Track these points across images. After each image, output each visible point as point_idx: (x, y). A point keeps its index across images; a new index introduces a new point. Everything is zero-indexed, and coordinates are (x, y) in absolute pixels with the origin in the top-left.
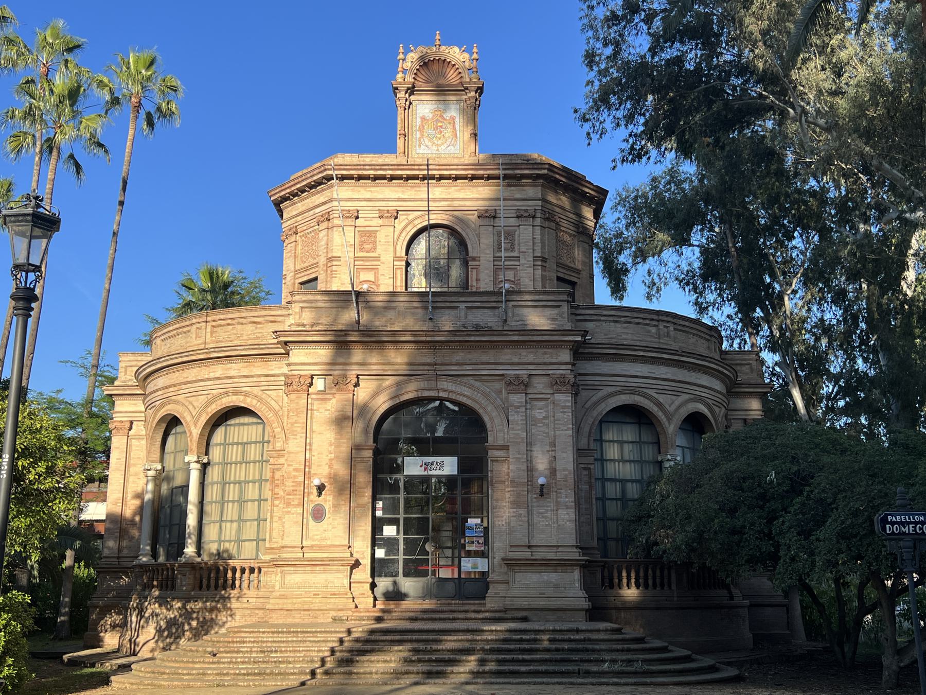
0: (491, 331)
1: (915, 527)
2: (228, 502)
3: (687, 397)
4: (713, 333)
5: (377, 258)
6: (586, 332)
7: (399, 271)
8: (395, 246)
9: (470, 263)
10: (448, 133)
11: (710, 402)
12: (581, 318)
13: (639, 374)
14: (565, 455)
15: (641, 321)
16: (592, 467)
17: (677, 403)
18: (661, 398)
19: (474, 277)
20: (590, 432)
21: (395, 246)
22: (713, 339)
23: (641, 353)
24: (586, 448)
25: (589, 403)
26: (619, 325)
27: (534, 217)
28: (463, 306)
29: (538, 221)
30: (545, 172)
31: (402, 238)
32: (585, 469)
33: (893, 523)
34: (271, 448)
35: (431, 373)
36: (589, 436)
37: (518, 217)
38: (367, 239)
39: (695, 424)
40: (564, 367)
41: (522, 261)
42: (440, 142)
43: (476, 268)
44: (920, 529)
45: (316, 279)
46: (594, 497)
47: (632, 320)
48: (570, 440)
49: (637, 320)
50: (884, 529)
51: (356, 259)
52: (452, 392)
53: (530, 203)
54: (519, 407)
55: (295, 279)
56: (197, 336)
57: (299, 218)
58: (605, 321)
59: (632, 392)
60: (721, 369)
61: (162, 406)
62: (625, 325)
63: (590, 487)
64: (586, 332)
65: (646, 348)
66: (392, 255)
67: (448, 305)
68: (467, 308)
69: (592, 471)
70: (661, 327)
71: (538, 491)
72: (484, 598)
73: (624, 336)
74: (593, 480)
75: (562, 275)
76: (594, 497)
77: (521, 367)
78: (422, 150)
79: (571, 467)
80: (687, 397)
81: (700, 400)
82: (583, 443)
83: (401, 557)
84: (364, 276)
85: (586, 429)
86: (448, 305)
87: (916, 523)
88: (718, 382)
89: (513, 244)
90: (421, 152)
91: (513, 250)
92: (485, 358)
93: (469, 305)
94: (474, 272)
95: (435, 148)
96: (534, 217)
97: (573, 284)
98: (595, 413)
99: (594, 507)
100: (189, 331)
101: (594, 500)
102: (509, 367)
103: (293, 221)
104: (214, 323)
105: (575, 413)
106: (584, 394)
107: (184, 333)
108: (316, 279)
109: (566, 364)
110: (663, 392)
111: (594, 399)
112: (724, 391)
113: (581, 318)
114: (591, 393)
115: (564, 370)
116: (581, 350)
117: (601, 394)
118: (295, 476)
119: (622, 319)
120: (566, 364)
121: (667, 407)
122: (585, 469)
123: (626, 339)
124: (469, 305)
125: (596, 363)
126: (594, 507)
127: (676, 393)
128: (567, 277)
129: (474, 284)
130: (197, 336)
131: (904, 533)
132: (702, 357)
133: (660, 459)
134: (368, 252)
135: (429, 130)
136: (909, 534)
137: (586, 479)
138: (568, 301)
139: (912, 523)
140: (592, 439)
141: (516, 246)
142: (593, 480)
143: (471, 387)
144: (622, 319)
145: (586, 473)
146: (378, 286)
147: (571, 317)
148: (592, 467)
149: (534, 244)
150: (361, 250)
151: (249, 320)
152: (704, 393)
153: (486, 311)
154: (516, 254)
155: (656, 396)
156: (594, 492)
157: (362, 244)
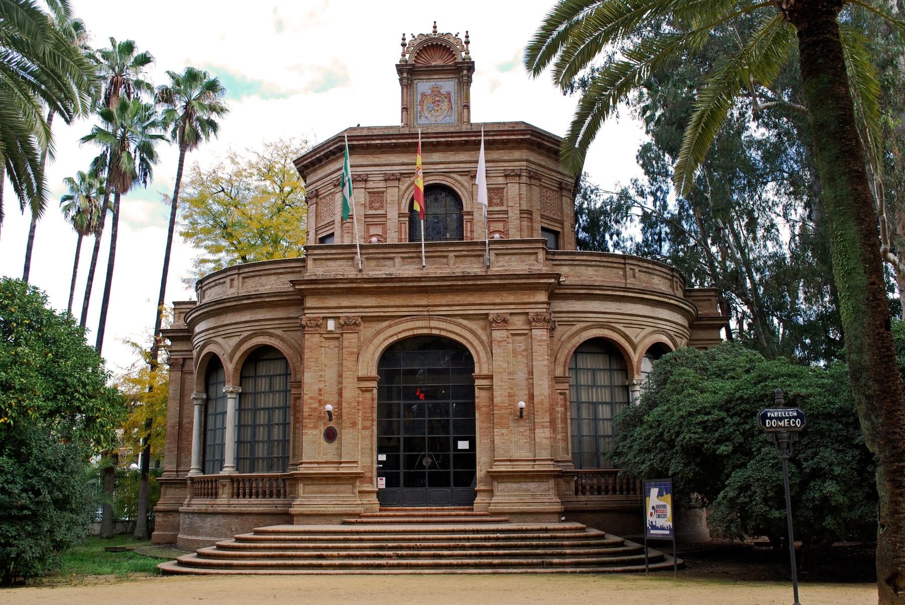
0: (476, 277)
1: (789, 421)
2: (258, 459)
3: (652, 329)
4: (675, 274)
5: (385, 216)
6: (559, 275)
7: (403, 226)
8: (399, 204)
9: (465, 217)
10: (445, 105)
11: (672, 333)
12: (558, 263)
13: (608, 311)
14: (541, 382)
15: (609, 264)
16: (567, 392)
17: (642, 335)
18: (628, 331)
19: (469, 228)
20: (565, 362)
21: (399, 204)
22: (675, 279)
23: (610, 293)
24: (562, 375)
25: (565, 337)
26: (590, 269)
27: (519, 176)
28: (452, 254)
29: (524, 179)
30: (529, 137)
31: (406, 195)
32: (561, 394)
33: (771, 418)
34: (293, 379)
35: (426, 313)
36: (565, 365)
37: (506, 176)
38: (376, 196)
39: (656, 351)
40: (541, 306)
41: (510, 214)
42: (438, 114)
43: (471, 221)
44: (794, 423)
45: (332, 235)
46: (569, 417)
47: (602, 264)
48: (546, 369)
49: (606, 264)
50: (764, 424)
51: (366, 216)
52: (444, 330)
53: (517, 164)
54: (501, 342)
55: (316, 235)
56: (231, 286)
57: (319, 183)
58: (579, 265)
59: (602, 326)
60: (681, 305)
61: (204, 346)
62: (596, 268)
63: (566, 409)
64: (559, 275)
65: (614, 288)
66: (397, 212)
67: (438, 254)
68: (456, 256)
69: (568, 395)
70: (628, 270)
71: (518, 413)
72: (472, 504)
73: (594, 278)
74: (568, 403)
75: (546, 226)
76: (569, 417)
77: (502, 307)
78: (422, 121)
79: (546, 392)
80: (652, 329)
81: (663, 332)
82: (559, 372)
83: (402, 470)
84: (374, 230)
85: (562, 358)
86: (438, 254)
87: (790, 418)
88: (679, 316)
89: (502, 200)
90: (421, 122)
91: (502, 204)
92: (471, 299)
93: (458, 253)
94: (469, 224)
95: (433, 119)
96: (519, 176)
97: (556, 234)
98: (570, 346)
99: (569, 425)
100: (225, 282)
101: (569, 421)
102: (492, 307)
103: (314, 185)
104: (244, 275)
105: (550, 347)
106: (559, 330)
107: (220, 284)
108: (332, 235)
109: (542, 303)
110: (629, 325)
111: (569, 333)
112: (686, 324)
113: (558, 263)
114: (566, 328)
115: (541, 309)
116: (557, 291)
117: (575, 328)
118: (311, 404)
119: (593, 263)
120: (542, 303)
121: (633, 339)
122: (561, 394)
123: (596, 281)
124: (458, 253)
125: (570, 302)
126: (569, 425)
127: (641, 327)
128: (550, 227)
129: (469, 235)
130: (231, 286)
131: (781, 427)
132: (663, 295)
133: (627, 383)
134: (376, 210)
135: (428, 103)
136: (785, 427)
137: (562, 402)
138: (543, 248)
139: (786, 418)
140: (567, 368)
141: (505, 201)
142: (568, 403)
143: (460, 325)
144: (593, 263)
145: (562, 397)
146: (386, 239)
147: (548, 262)
148: (567, 392)
149: (520, 199)
150: (371, 208)
151: (273, 271)
152: (667, 326)
153: (472, 258)
154: (504, 208)
155: (623, 329)
156: (569, 414)
157: (371, 202)
